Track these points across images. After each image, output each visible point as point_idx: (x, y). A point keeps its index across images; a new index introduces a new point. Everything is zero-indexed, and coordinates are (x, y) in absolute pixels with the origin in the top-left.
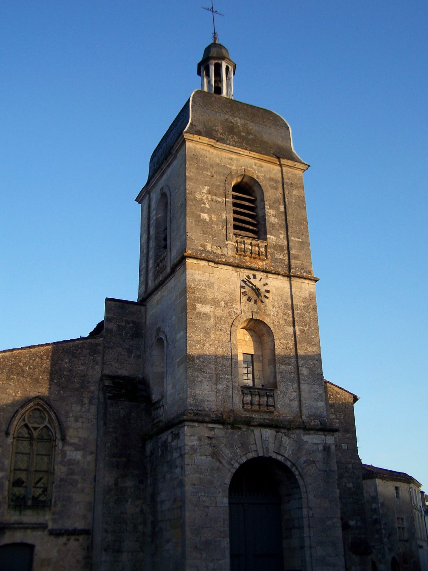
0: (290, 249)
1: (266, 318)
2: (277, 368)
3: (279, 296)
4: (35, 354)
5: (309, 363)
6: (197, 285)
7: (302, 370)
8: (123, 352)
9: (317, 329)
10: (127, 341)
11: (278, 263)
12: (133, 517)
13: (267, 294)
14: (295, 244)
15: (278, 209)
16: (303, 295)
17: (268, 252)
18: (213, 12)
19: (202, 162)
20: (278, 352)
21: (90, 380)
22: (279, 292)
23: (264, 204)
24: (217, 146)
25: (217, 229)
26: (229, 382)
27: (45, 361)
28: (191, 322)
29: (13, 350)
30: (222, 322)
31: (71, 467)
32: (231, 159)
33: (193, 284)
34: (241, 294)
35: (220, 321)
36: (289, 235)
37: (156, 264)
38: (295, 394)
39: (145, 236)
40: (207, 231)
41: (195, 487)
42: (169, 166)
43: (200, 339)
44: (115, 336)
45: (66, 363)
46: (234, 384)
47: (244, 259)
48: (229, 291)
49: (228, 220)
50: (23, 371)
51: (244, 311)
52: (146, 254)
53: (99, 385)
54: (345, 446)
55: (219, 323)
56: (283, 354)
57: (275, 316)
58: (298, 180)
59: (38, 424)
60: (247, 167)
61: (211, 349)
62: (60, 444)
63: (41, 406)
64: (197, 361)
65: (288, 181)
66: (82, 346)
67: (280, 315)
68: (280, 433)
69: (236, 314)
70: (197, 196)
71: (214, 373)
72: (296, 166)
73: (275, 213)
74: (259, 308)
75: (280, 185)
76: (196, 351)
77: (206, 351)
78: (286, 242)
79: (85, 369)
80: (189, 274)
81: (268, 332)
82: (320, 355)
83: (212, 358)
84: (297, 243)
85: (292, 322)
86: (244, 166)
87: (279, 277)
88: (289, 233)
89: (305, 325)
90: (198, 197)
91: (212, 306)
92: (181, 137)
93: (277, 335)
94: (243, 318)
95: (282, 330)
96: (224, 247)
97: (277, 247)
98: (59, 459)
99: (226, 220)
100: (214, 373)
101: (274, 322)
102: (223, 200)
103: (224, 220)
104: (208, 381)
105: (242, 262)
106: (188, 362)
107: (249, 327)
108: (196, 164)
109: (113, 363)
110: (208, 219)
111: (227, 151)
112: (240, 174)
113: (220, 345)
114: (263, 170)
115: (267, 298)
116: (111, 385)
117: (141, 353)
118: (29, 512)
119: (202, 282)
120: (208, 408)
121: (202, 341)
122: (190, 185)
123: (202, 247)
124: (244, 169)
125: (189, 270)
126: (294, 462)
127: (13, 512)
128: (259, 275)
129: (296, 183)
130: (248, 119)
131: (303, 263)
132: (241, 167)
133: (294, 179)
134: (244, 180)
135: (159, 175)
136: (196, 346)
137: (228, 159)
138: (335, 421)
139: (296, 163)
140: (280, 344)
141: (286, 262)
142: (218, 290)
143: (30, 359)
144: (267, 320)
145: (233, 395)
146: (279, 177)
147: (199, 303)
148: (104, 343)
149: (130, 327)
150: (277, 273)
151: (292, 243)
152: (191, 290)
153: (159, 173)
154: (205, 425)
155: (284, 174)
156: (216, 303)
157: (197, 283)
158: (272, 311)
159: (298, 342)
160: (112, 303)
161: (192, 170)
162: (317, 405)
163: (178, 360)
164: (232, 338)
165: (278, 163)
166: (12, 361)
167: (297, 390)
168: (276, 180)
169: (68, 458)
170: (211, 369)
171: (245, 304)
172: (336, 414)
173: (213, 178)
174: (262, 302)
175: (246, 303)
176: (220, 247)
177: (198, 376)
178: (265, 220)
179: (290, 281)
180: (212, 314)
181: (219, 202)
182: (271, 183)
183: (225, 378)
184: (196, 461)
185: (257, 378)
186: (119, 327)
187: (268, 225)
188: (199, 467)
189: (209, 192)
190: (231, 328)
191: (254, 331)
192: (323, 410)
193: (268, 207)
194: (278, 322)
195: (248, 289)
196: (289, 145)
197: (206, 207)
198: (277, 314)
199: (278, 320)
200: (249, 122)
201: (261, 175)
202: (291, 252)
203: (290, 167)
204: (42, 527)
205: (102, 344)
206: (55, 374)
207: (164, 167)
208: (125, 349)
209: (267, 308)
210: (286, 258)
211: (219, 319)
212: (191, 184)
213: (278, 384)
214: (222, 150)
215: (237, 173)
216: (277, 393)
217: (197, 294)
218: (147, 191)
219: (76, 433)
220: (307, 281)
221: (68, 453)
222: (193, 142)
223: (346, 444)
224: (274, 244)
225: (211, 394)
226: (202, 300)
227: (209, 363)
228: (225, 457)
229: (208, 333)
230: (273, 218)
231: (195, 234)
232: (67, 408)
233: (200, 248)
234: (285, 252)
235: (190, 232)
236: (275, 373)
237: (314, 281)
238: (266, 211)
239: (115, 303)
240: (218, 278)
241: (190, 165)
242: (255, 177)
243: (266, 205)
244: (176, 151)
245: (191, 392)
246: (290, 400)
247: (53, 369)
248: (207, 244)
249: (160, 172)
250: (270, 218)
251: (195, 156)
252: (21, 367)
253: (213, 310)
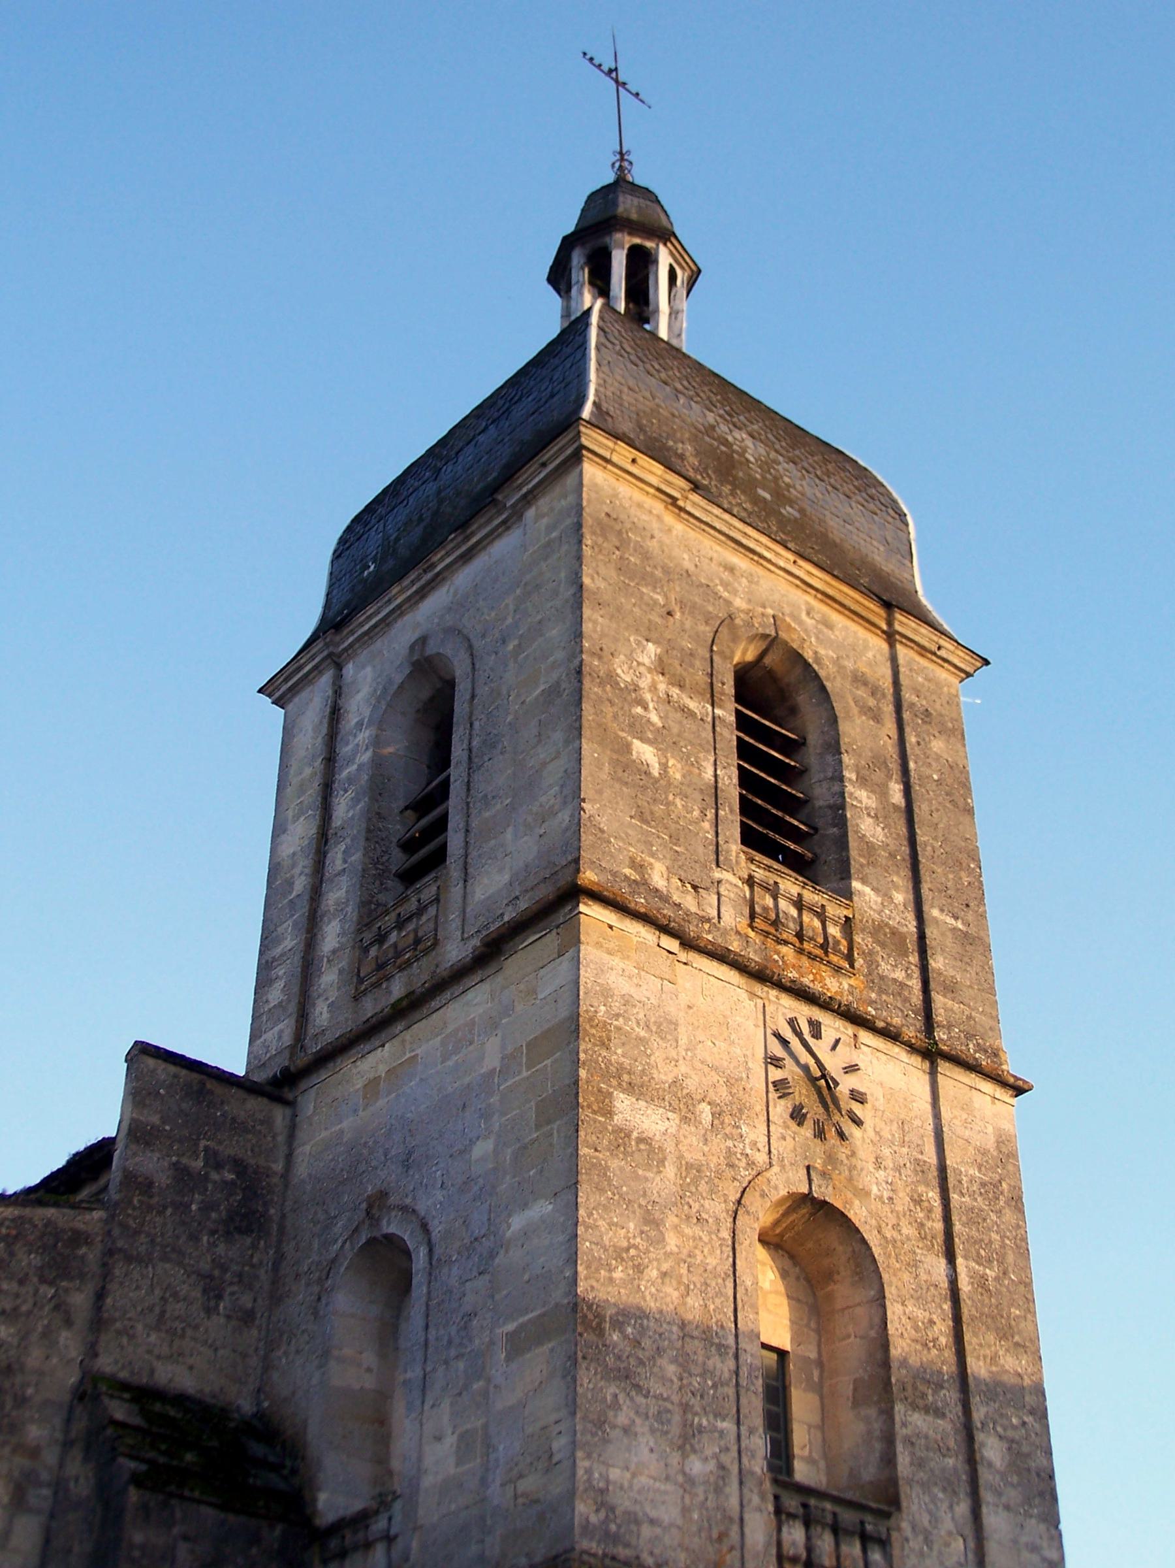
0: (929, 952)
1: (857, 1202)
2: (897, 1418)
3: (895, 1123)
6: (617, 1016)
8: (185, 1287)
9: (1028, 1285)
10: (205, 1238)
11: (887, 994)
13: (857, 1108)
14: (943, 934)
15: (882, 792)
16: (977, 1140)
17: (856, 945)
18: (617, 81)
20: (899, 1350)
21: (30, 1391)
22: (897, 1109)
23: (841, 762)
24: (689, 508)
25: (684, 813)
26: (727, 1449)
28: (594, 1165)
30: (703, 1187)
32: (731, 569)
33: (603, 1008)
34: (771, 1086)
35: (695, 1182)
36: (924, 897)
37: (368, 936)
38: (962, 1547)
39: (302, 830)
40: (652, 813)
42: (467, 557)
43: (625, 1244)
44: (160, 1213)
46: (745, 1460)
47: (778, 953)
48: (725, 1064)
49: (723, 791)
51: (781, 1160)
52: (307, 897)
53: (68, 1421)
55: (694, 1190)
56: (914, 1361)
57: (883, 1203)
58: (944, 703)
60: (783, 614)
61: (667, 1295)
64: (615, 1338)
65: (914, 699)
66: (14, 1232)
67: (903, 1201)
69: (751, 1164)
70: (619, 671)
71: (675, 1398)
72: (942, 653)
73: (874, 806)
74: (830, 1158)
75: (888, 709)
76: (610, 1289)
77: (648, 1298)
78: (915, 923)
79: (15, 1341)
80: (588, 966)
81: (857, 1265)
82: (1040, 1392)
83: (671, 1332)
84: (949, 934)
85: (940, 1239)
86: (772, 608)
87: (897, 1050)
88: (925, 888)
90: (625, 676)
91: (670, 1115)
92: (562, 441)
93: (894, 1280)
94: (776, 1188)
95: (909, 1264)
96: (706, 889)
97: (885, 935)
99: (716, 788)
100: (675, 1398)
101: (883, 1225)
102: (703, 711)
105: (768, 958)
106: (581, 1335)
107: (781, 1235)
108: (617, 552)
109: (139, 1327)
110: (657, 765)
111: (717, 534)
112: (761, 631)
113: (695, 1285)
114: (832, 637)
115: (858, 1122)
116: (137, 1421)
117: (255, 1300)
119: (635, 1006)
120: (651, 1553)
121: (632, 1252)
122: (595, 622)
123: (635, 871)
124: (774, 617)
125: (589, 948)
128: (833, 1027)
129: (941, 715)
130: (777, 446)
131: (974, 1014)
132: (764, 607)
133: (934, 697)
134: (767, 660)
135: (409, 593)
136: (610, 1271)
137: (720, 564)
139: (943, 642)
141: (917, 997)
142: (689, 1053)
144: (857, 1213)
145: (741, 1512)
146: (883, 677)
147: (624, 1091)
148: (109, 1233)
149: (225, 1182)
150: (890, 1035)
151: (935, 932)
152: (593, 1031)
153: (413, 583)
155: (902, 669)
157: (616, 1006)
158: (875, 1181)
159: (968, 1325)
160: (164, 1070)
161: (602, 570)
163: (511, 1327)
164: (738, 1261)
165: (885, 627)
167: (968, 1531)
168: (877, 688)
170: (664, 1380)
171: (783, 1131)
173: (671, 618)
174: (842, 1135)
175: (787, 1127)
176: (695, 887)
177: (615, 1405)
178: (841, 822)
179: (933, 1073)
180: (669, 1147)
181: (691, 714)
182: (859, 692)
183: (714, 1429)
185: (802, 1458)
186: (181, 1173)
187: (853, 843)
189: (661, 668)
190: (735, 1218)
191: (792, 1257)
193: (854, 777)
194: (896, 1227)
195: (793, 1072)
196: (910, 578)
197: (649, 721)
198: (891, 1194)
199: (894, 1222)
200: (781, 459)
203: (923, 650)
205: (99, 1238)
207: (441, 560)
208: (194, 1277)
209: (859, 1164)
210: (915, 984)
211: (692, 1171)
212: (600, 620)
213: (904, 1489)
214: (703, 526)
215: (749, 624)
216: (899, 1529)
218: (330, 655)
220: (987, 1087)
222: (609, 467)
224: (873, 920)
225: (666, 1492)
226: (637, 1080)
229: (656, 1224)
230: (870, 820)
231: (610, 811)
234: (911, 959)
235: (594, 801)
236: (889, 1439)
237: (1011, 1092)
238: (847, 789)
239: (172, 1069)
240: (689, 1007)
241: (596, 549)
242: (808, 655)
243: (847, 766)
244: (525, 496)
245: (589, 1471)
248: (652, 860)
249: (418, 578)
250: (860, 817)
251: (612, 523)
253: (672, 1130)
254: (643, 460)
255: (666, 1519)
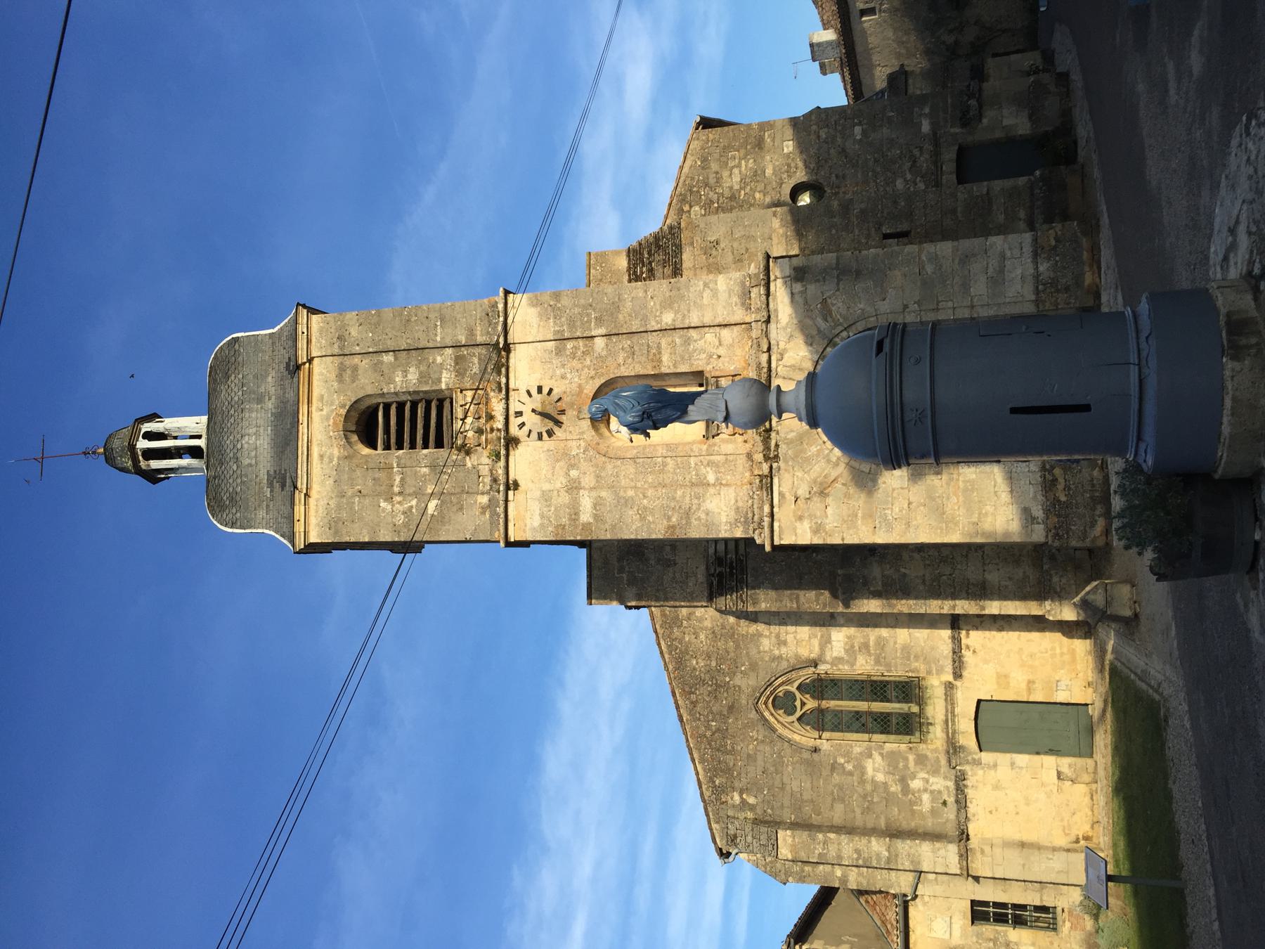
1: (585, 391)
4: (691, 713)
5: (652, 308)
6: (550, 521)
7: (666, 324)
12: (929, 565)
13: (545, 391)
19: (339, 514)
27: (700, 697)
29: (688, 746)
31: (857, 648)
32: (321, 457)
40: (457, 503)
41: (878, 526)
45: (697, 663)
50: (718, 730)
54: (788, 148)
59: (795, 700)
62: (822, 668)
63: (768, 698)
67: (575, 363)
68: (779, 369)
74: (572, 405)
88: (431, 345)
89: (588, 315)
90: (400, 519)
98: (846, 667)
103: (431, 470)
104: (704, 501)
112: (344, 440)
115: (551, 390)
118: (929, 711)
121: (640, 512)
126: (826, 342)
127: (931, 736)
138: (743, 169)
140: (627, 366)
143: (699, 719)
154: (776, 510)
156: (574, 487)
162: (725, 291)
165: (307, 364)
166: (705, 749)
169: (842, 654)
170: (684, 496)
172: (733, 167)
181: (402, 479)
184: (835, 525)
188: (846, 519)
189: (390, 499)
192: (731, 279)
201: (338, 399)
202: (463, 343)
203: (309, 342)
204: (949, 687)
206: (716, 680)
210: (477, 351)
217: (565, 521)
219: (804, 643)
221: (835, 654)
223: (785, 143)
227: (674, 498)
228: (826, 471)
232: (767, 659)
233: (488, 516)
234: (465, 353)
242: (343, 412)
246: (720, 345)
247: (710, 683)
252: (713, 734)
254: (296, 517)
255: (734, 494)
